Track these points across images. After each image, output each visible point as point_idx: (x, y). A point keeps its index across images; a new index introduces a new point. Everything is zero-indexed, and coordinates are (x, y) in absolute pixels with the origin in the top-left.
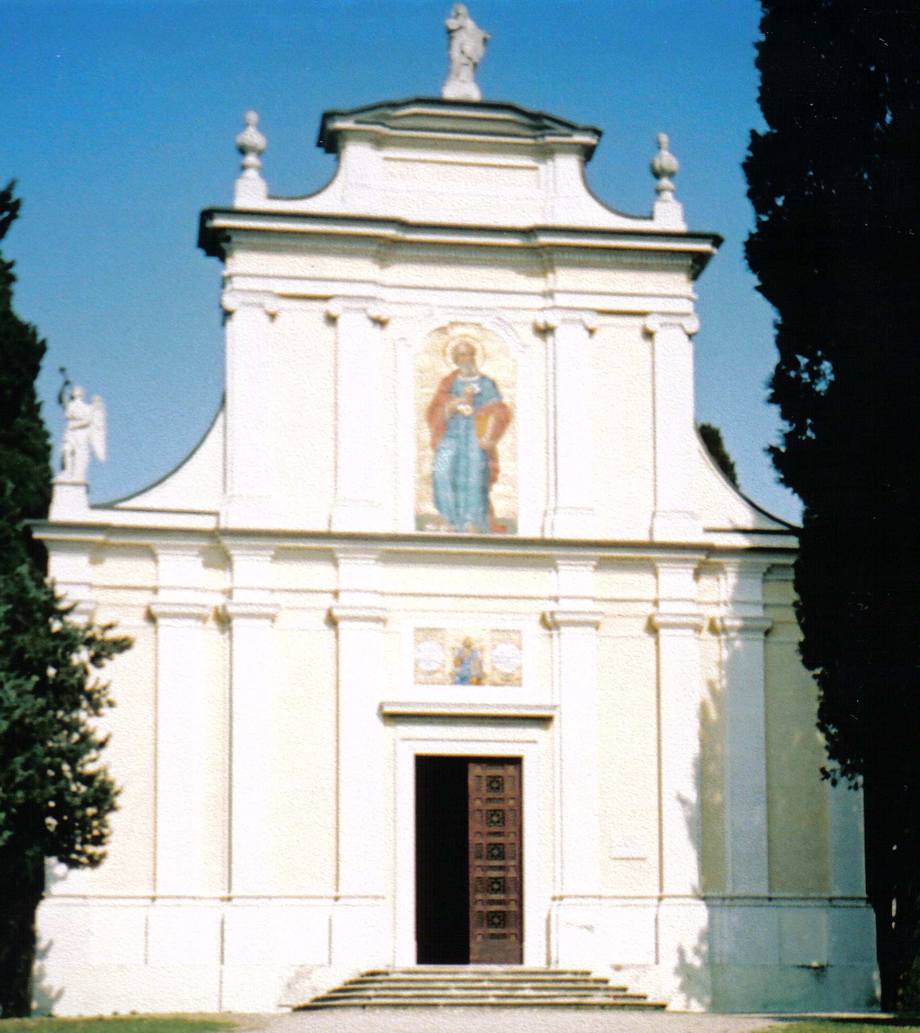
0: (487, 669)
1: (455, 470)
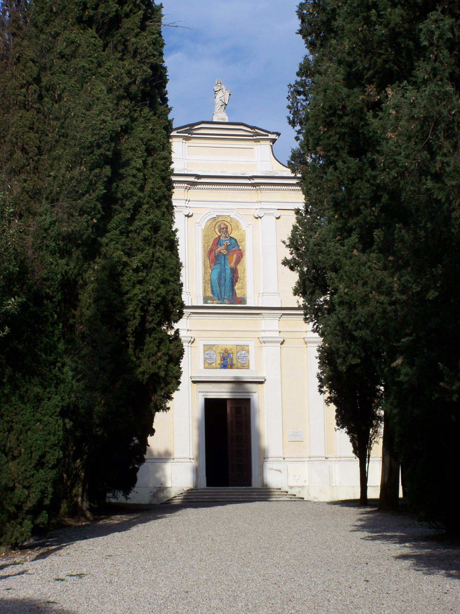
0: (235, 362)
1: (220, 278)
